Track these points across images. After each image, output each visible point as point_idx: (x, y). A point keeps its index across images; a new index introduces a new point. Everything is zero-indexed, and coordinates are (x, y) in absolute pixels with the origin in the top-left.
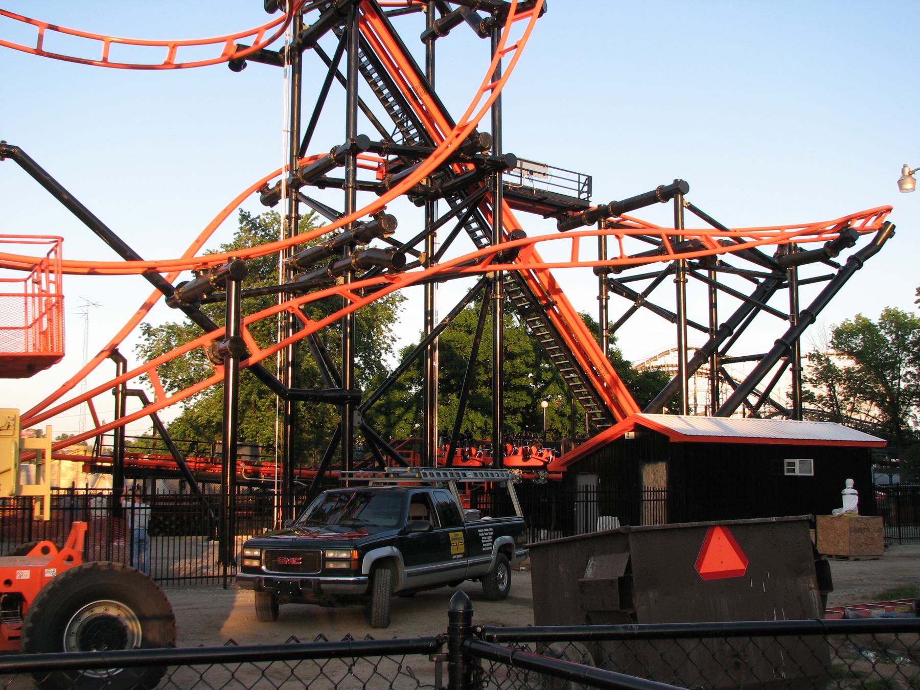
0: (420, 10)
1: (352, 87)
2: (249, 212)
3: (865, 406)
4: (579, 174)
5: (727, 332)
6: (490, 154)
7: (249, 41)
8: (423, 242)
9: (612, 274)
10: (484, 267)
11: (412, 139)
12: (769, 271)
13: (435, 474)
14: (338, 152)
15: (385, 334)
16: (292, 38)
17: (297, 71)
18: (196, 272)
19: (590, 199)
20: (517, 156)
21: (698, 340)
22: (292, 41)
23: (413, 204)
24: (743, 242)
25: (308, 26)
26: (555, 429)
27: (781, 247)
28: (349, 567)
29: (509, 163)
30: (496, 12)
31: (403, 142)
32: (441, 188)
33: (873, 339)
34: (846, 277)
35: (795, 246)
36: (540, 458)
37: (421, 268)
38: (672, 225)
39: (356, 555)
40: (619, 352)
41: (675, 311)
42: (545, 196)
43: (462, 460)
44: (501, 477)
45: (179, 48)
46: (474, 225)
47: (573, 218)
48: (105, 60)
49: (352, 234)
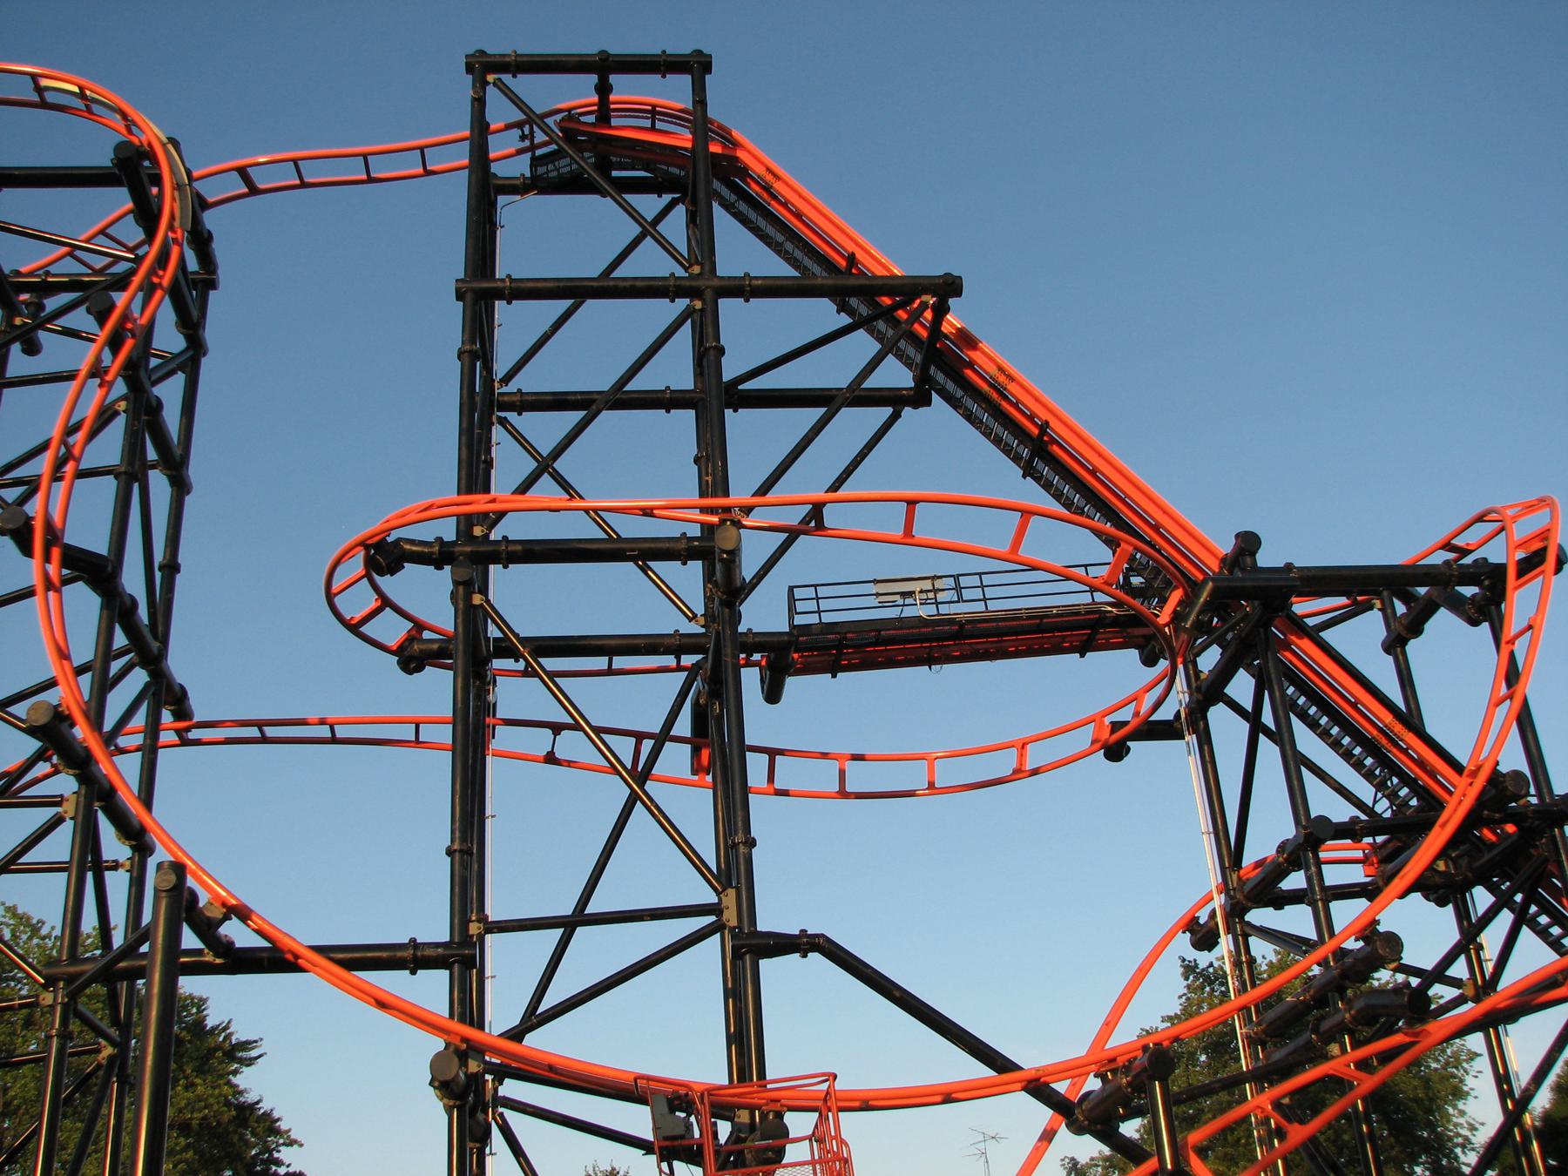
0: (1371, 608)
2: (1195, 960)
6: (1534, 800)
7: (1125, 714)
11: (1405, 804)
14: (1289, 848)
15: (1455, 1120)
17: (1205, 741)
18: (1101, 1075)
22: (1187, 700)
25: (1207, 673)
30: (1487, 582)
37: (1470, 1005)
45: (1029, 746)
46: (1544, 919)
48: (931, 785)
49: (1335, 972)
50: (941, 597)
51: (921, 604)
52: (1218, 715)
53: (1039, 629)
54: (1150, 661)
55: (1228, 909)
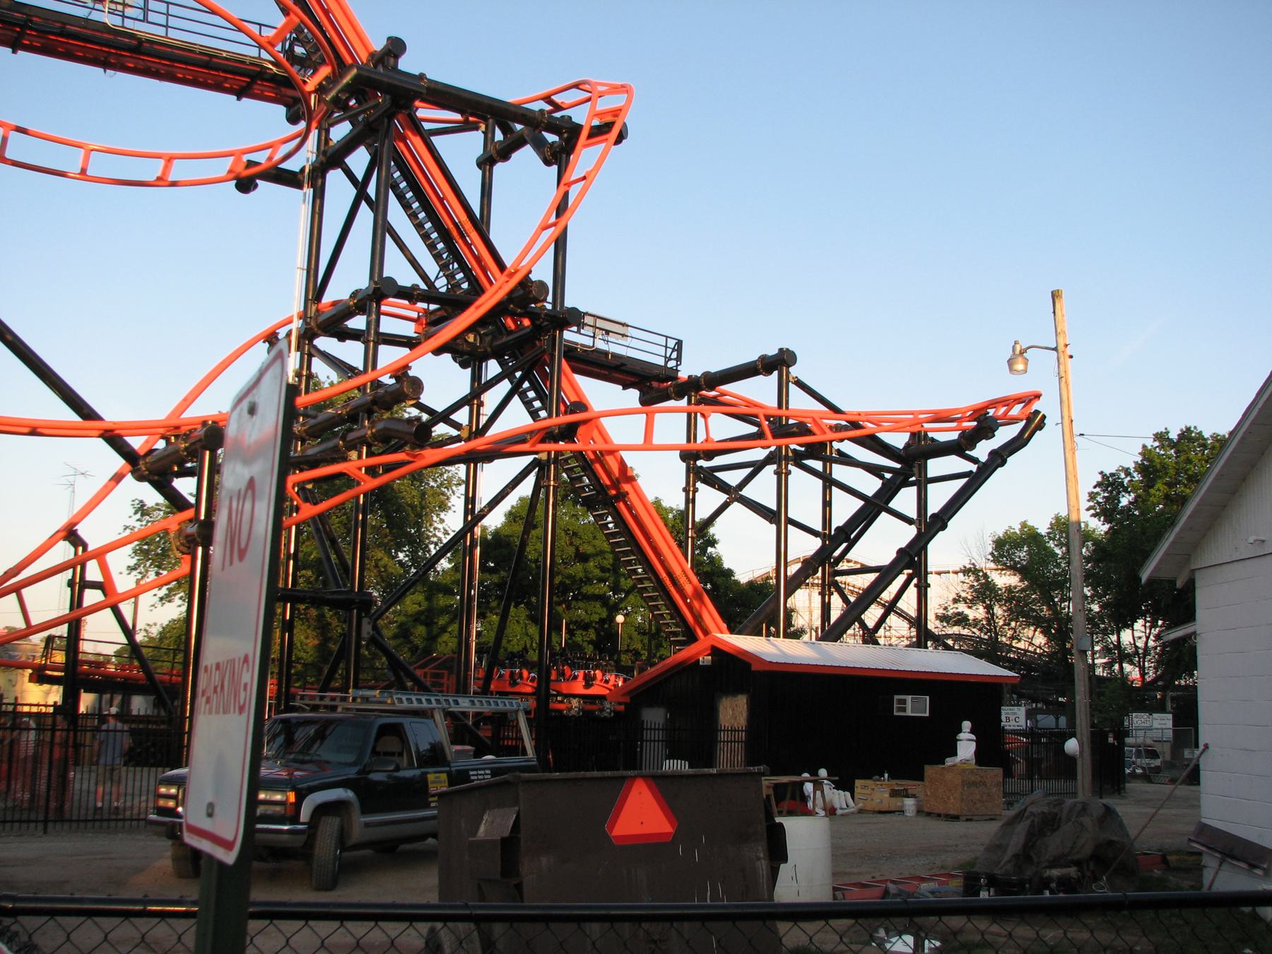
0: (477, 129)
1: (380, 222)
3: (1029, 632)
4: (667, 337)
5: (843, 537)
7: (261, 157)
8: (466, 409)
9: (702, 461)
10: (533, 446)
11: (458, 285)
12: (898, 466)
13: (423, 700)
14: (360, 296)
15: (436, 525)
16: (315, 156)
17: (319, 195)
19: (679, 368)
20: (582, 309)
21: (803, 546)
22: (314, 159)
23: (457, 365)
24: (861, 427)
26: (634, 649)
27: (913, 435)
28: (283, 812)
29: (575, 318)
30: (566, 135)
31: (448, 288)
32: (491, 347)
33: (1039, 553)
34: (988, 473)
35: (926, 435)
36: (606, 685)
38: (773, 403)
39: (292, 797)
40: (720, 559)
41: (774, 507)
42: (624, 362)
43: (510, 683)
44: (508, 707)
47: (659, 390)
48: (83, 171)
49: (369, 398)
50: (129, 12)
51: (109, 12)
52: (335, 178)
53: (206, 65)
54: (293, 119)
55: (302, 332)
